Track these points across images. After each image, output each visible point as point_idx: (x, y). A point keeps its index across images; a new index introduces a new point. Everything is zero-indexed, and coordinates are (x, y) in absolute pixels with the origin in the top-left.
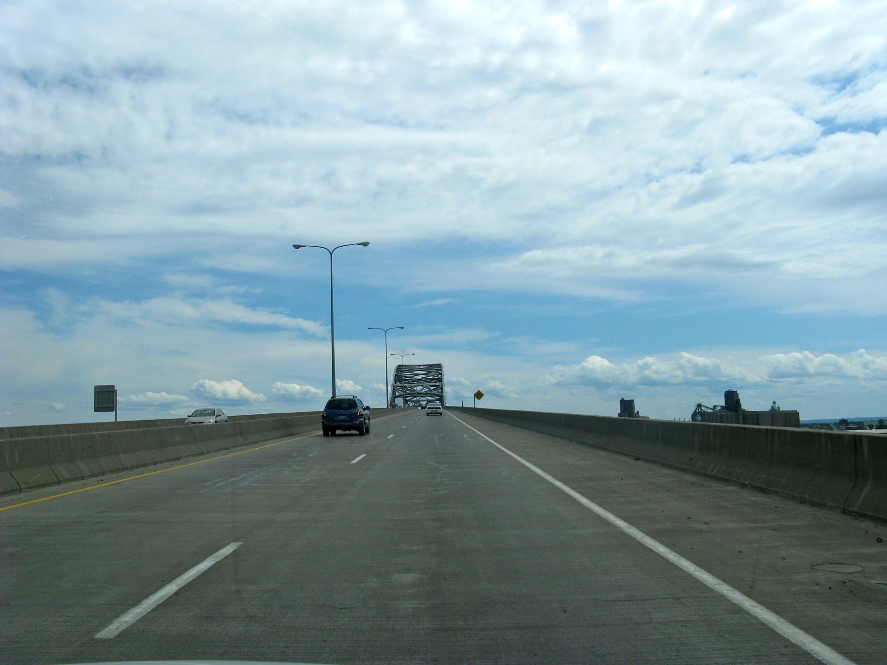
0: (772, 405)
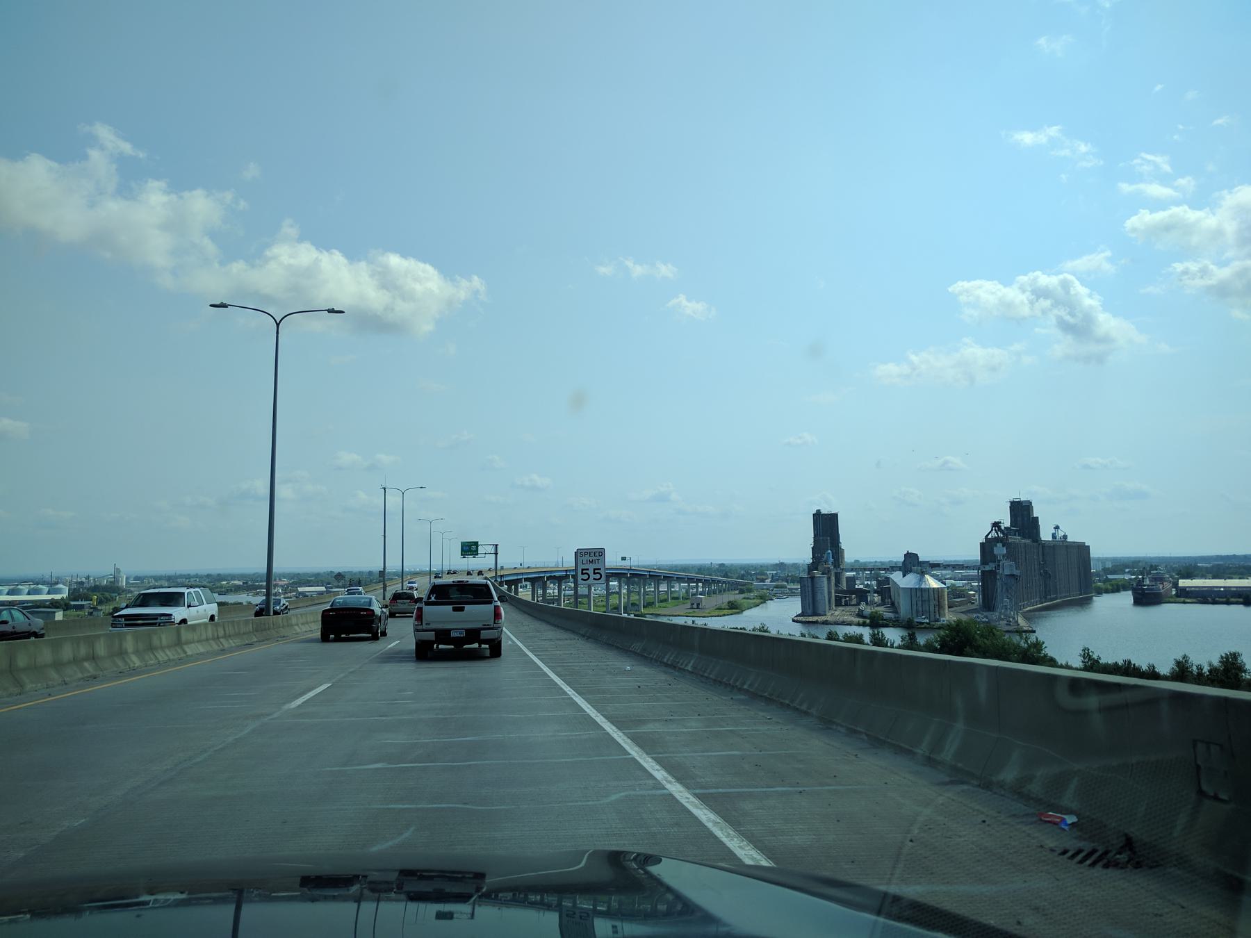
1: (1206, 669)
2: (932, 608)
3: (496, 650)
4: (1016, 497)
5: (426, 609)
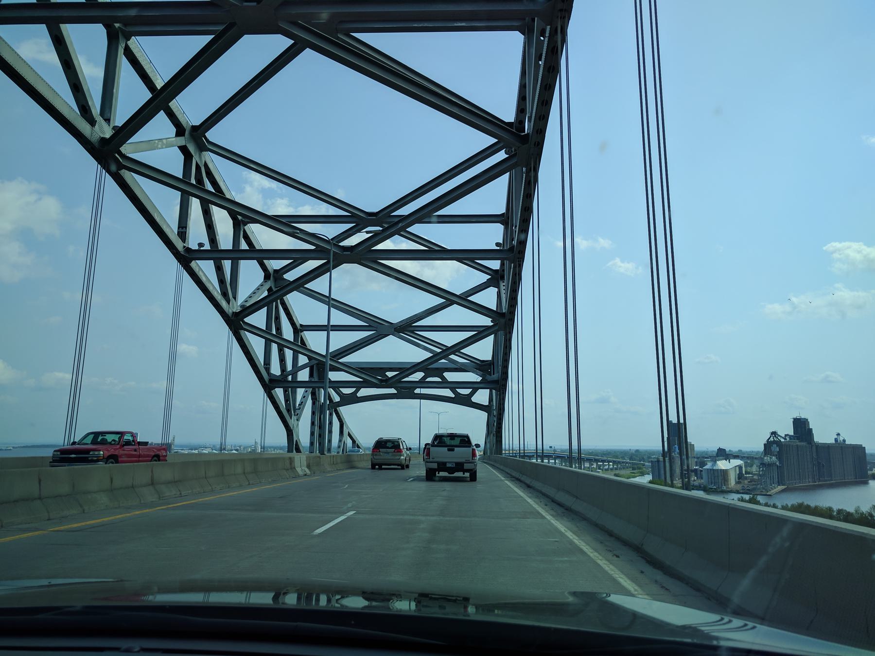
1: (790, 506)
2: (720, 481)
3: (473, 477)
4: (796, 415)
5: (432, 449)
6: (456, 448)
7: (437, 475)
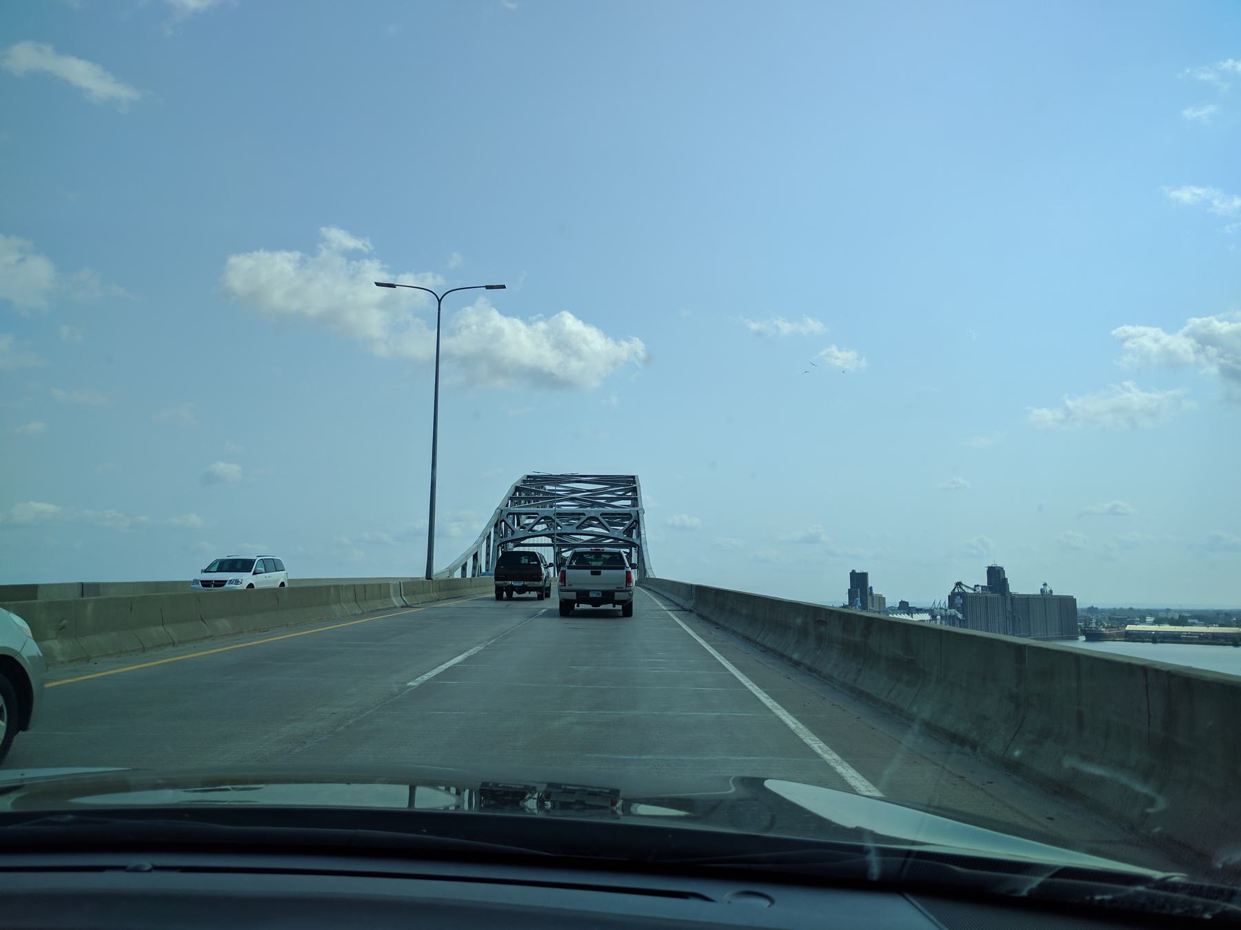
0: (1043, 587)
3: (628, 611)
5: (569, 572)
6: (602, 571)
7: (576, 607)
